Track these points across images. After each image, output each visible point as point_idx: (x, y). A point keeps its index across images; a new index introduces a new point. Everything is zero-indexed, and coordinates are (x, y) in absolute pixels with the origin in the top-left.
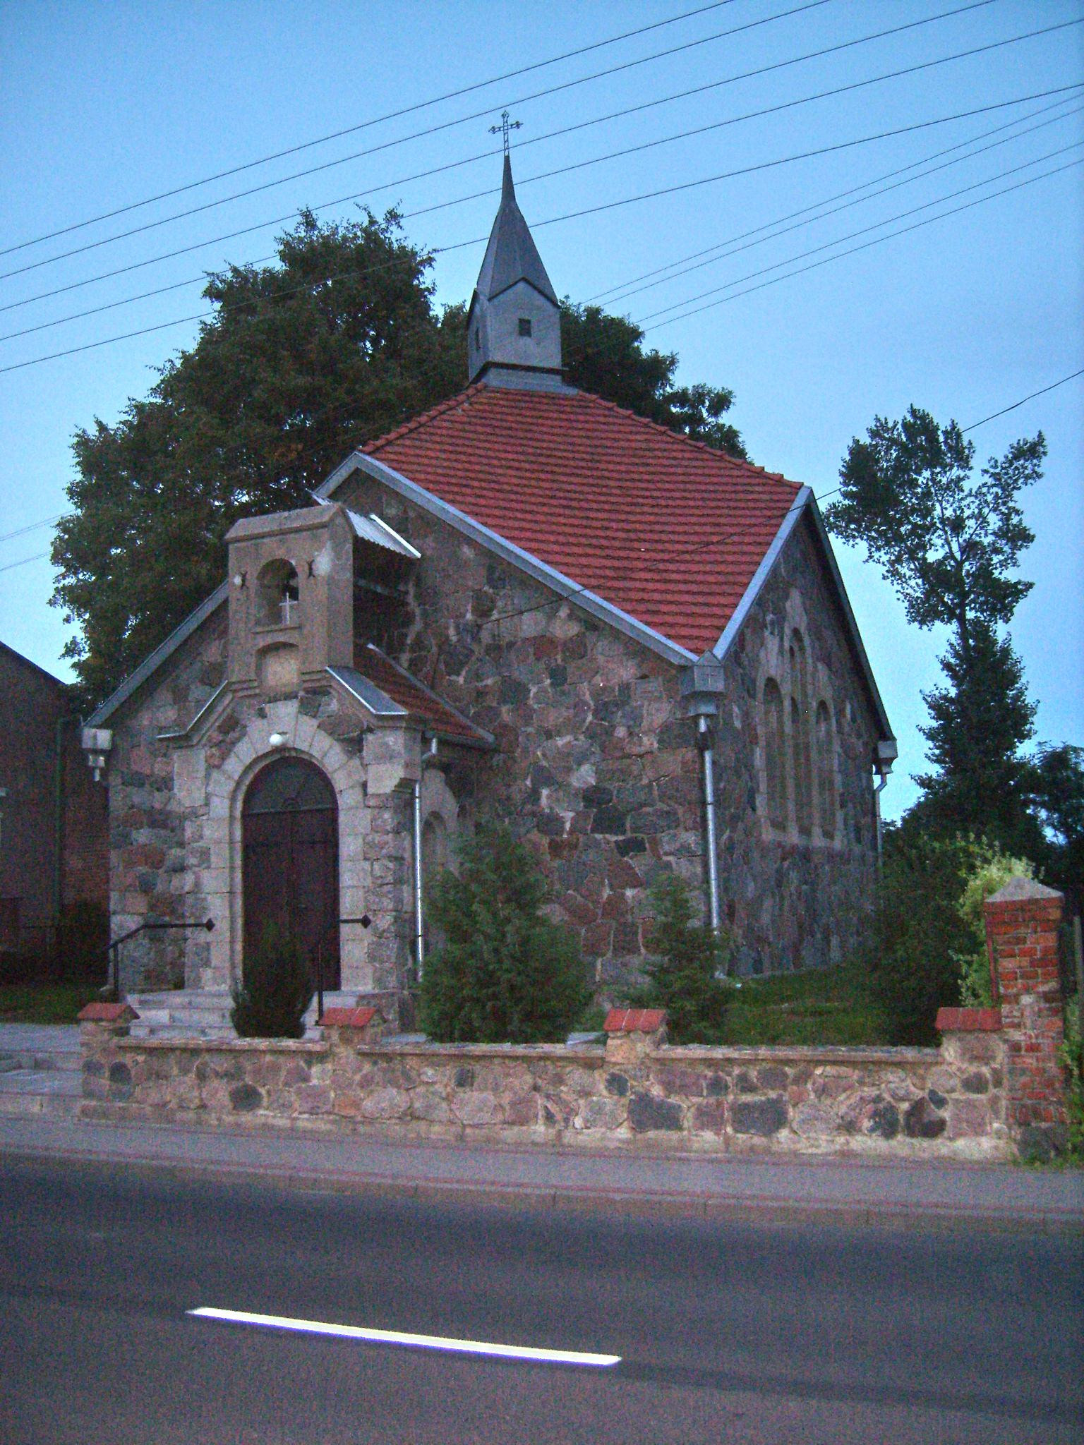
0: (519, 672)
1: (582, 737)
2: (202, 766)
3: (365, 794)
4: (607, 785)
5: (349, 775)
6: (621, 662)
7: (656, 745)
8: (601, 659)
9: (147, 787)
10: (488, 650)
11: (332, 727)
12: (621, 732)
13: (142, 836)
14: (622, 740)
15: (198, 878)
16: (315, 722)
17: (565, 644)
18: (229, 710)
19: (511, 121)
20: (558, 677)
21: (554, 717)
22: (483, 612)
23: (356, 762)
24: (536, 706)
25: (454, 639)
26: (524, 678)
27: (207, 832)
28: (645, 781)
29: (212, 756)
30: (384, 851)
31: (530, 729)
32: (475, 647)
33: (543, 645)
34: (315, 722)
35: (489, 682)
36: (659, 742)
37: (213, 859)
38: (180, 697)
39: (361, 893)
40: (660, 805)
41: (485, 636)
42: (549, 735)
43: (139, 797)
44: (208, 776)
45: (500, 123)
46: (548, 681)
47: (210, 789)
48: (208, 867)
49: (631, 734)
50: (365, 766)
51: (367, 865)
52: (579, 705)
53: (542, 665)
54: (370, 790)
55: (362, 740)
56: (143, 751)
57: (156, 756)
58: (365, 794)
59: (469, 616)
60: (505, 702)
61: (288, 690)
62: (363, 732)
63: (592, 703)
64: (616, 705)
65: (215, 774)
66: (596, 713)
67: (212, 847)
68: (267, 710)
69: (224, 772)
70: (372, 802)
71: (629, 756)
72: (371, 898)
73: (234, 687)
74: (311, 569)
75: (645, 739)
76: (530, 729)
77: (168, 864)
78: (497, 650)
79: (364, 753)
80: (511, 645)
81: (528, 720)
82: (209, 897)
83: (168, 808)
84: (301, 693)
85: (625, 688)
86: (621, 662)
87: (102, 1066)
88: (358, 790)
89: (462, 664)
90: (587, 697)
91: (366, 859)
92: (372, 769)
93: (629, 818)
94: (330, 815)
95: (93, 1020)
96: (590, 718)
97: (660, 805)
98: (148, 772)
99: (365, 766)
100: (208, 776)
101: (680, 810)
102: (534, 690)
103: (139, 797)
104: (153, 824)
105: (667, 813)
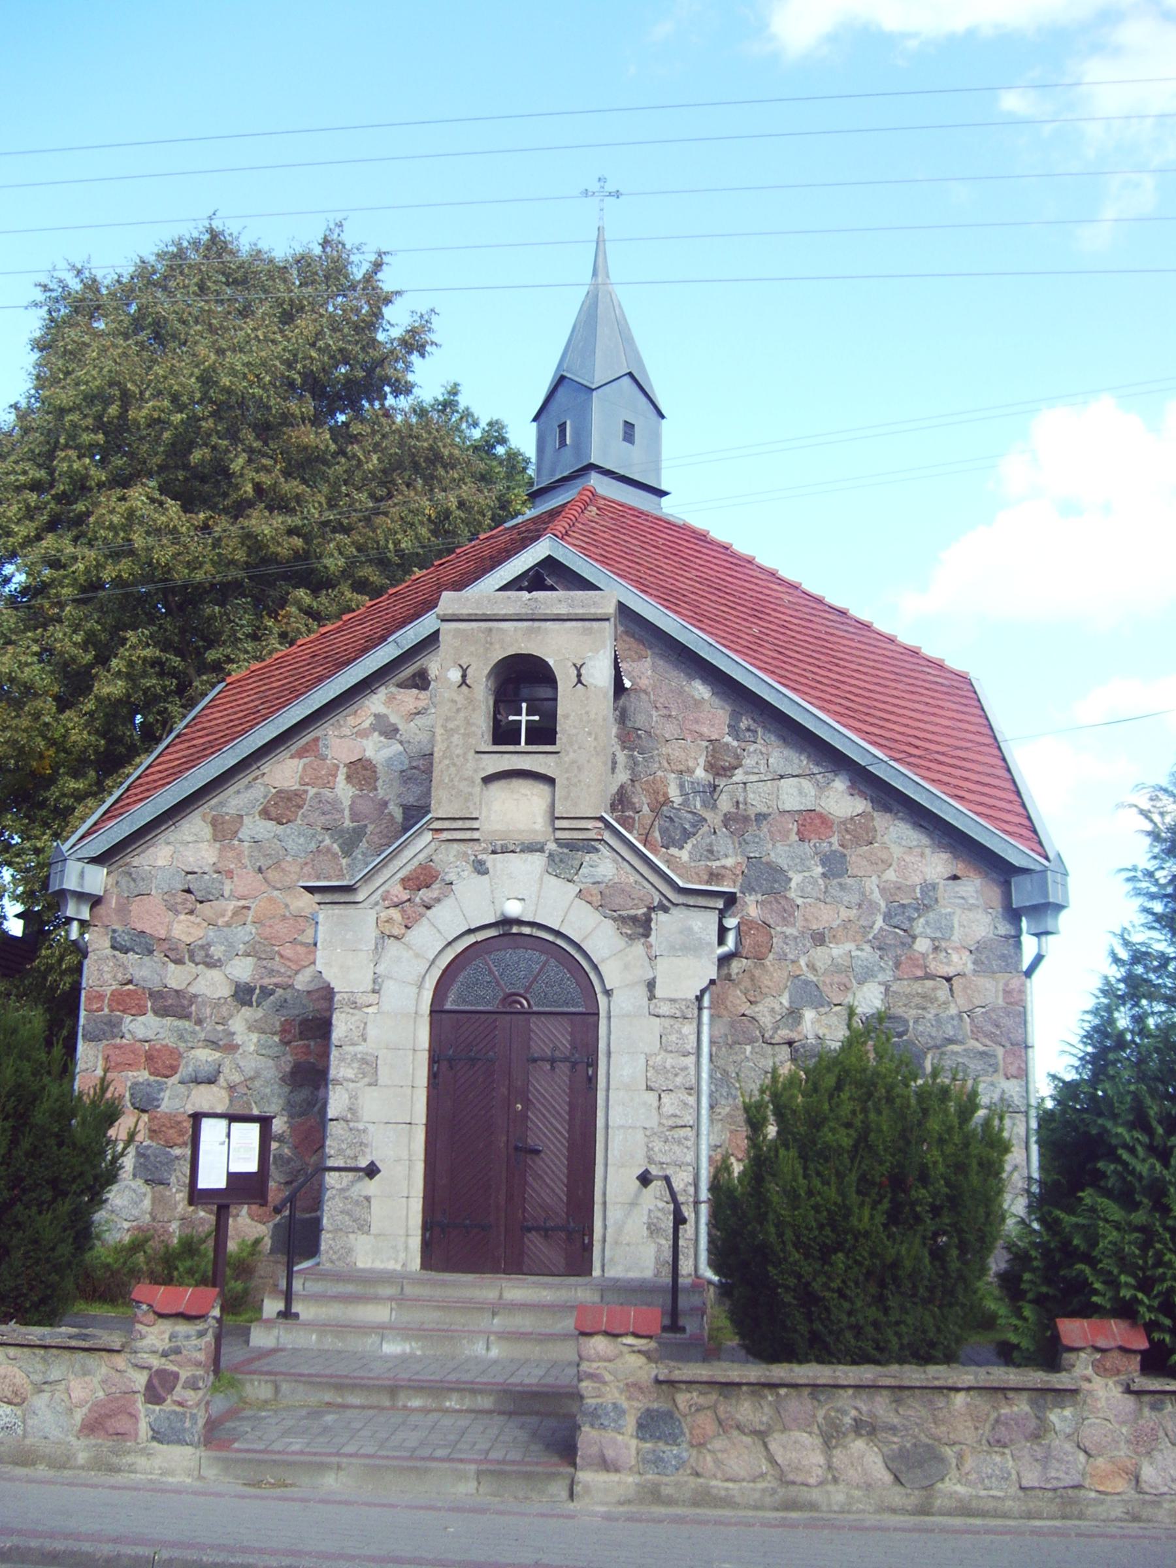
0: (779, 854)
1: (867, 947)
2: (371, 933)
3: (652, 997)
4: (899, 1011)
5: (627, 967)
6: (922, 855)
7: (970, 966)
8: (897, 851)
9: (158, 956)
10: (727, 820)
11: (603, 900)
12: (922, 945)
13: (145, 1027)
14: (924, 956)
15: (354, 1097)
16: (573, 889)
17: (844, 823)
18: (421, 856)
19: (610, 187)
20: (834, 866)
21: (826, 917)
22: (721, 768)
23: (638, 948)
24: (799, 901)
25: (677, 800)
26: (783, 863)
27: (372, 1032)
28: (953, 1011)
29: (389, 920)
30: (679, 1080)
31: (789, 931)
32: (708, 815)
33: (811, 823)
34: (573, 889)
35: (729, 862)
36: (975, 963)
37: (383, 1071)
38: (224, 831)
39: (640, 1136)
40: (973, 1043)
41: (725, 804)
42: (819, 939)
43: (146, 970)
44: (378, 950)
45: (594, 186)
46: (820, 870)
47: (381, 969)
48: (374, 1084)
49: (936, 949)
50: (652, 958)
51: (652, 1097)
52: (864, 904)
53: (807, 848)
54: (659, 992)
55: (648, 920)
56: (156, 901)
57: (177, 913)
58: (652, 997)
59: (700, 773)
60: (752, 890)
61: (528, 838)
62: (652, 909)
63: (883, 904)
64: (917, 910)
65: (393, 947)
66: (888, 917)
67: (382, 1053)
68: (489, 865)
69: (408, 946)
70: (665, 1009)
71: (929, 977)
72: (658, 1145)
73: (437, 825)
74: (579, 675)
75: (955, 957)
76: (789, 931)
77: (184, 1071)
78: (739, 822)
79: (652, 939)
80: (761, 817)
81: (787, 915)
82: (371, 1128)
83: (192, 990)
84: (552, 846)
85: (929, 888)
86: (922, 855)
87: (620, 1411)
88: (643, 991)
89: (687, 835)
90: (876, 896)
91: (649, 1088)
92: (662, 965)
93: (929, 1056)
94: (585, 1022)
95: (607, 1334)
96: (879, 922)
97: (973, 1043)
98: (162, 934)
99: (652, 958)
100: (378, 950)
101: (1000, 1052)
102: (796, 879)
103: (146, 970)
104: (162, 1012)
105: (983, 1054)
